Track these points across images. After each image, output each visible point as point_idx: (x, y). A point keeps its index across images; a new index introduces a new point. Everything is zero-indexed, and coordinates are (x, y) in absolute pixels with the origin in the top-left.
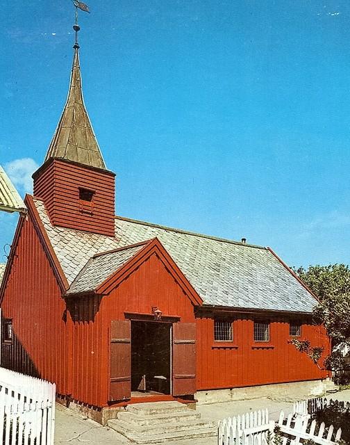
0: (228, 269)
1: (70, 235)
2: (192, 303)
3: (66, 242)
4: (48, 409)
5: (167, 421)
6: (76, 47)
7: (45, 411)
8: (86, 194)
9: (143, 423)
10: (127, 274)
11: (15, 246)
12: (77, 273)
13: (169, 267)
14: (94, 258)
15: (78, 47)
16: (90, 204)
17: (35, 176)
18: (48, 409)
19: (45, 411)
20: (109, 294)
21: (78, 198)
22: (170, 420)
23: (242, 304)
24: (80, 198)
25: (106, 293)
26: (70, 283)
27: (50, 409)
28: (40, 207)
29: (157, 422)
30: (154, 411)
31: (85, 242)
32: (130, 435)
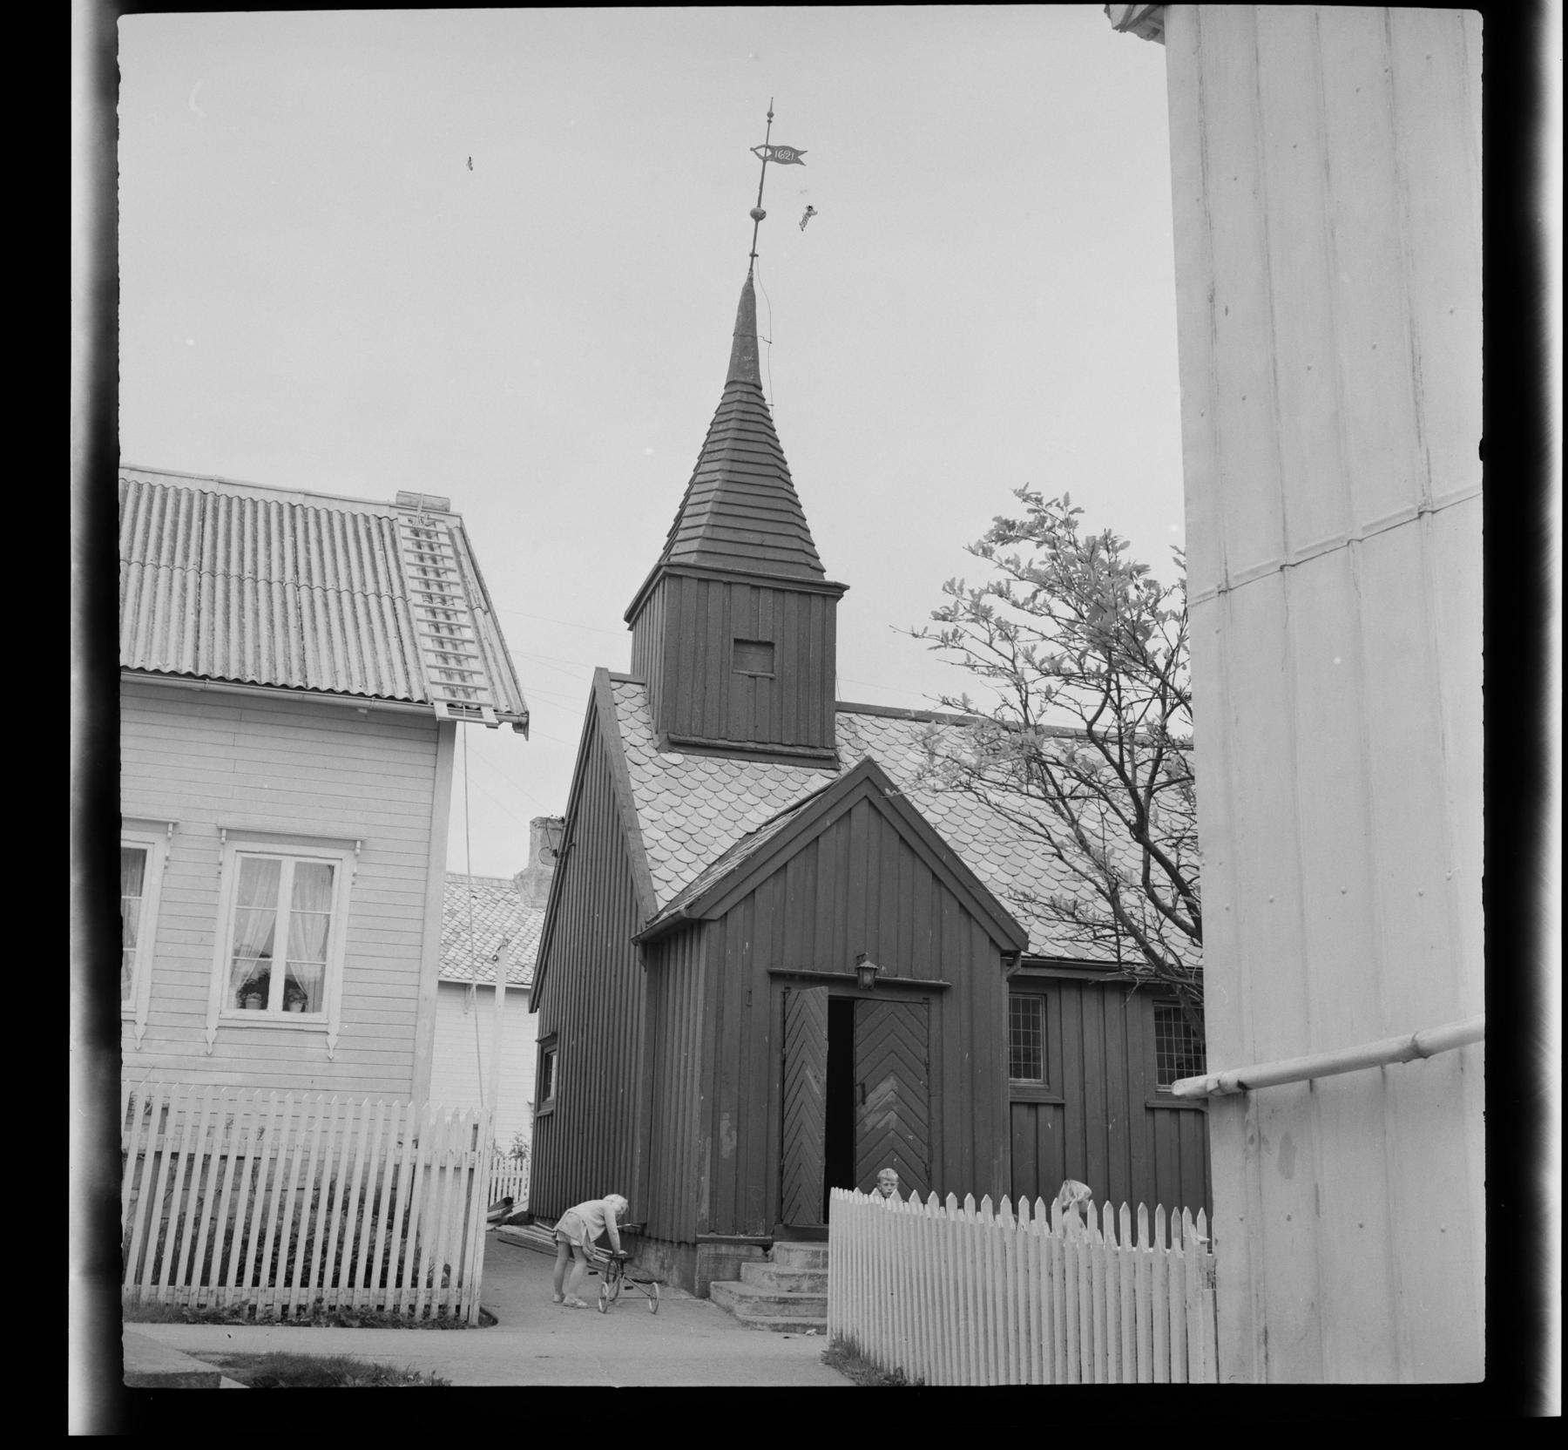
6: (758, 216)
25: (717, 913)
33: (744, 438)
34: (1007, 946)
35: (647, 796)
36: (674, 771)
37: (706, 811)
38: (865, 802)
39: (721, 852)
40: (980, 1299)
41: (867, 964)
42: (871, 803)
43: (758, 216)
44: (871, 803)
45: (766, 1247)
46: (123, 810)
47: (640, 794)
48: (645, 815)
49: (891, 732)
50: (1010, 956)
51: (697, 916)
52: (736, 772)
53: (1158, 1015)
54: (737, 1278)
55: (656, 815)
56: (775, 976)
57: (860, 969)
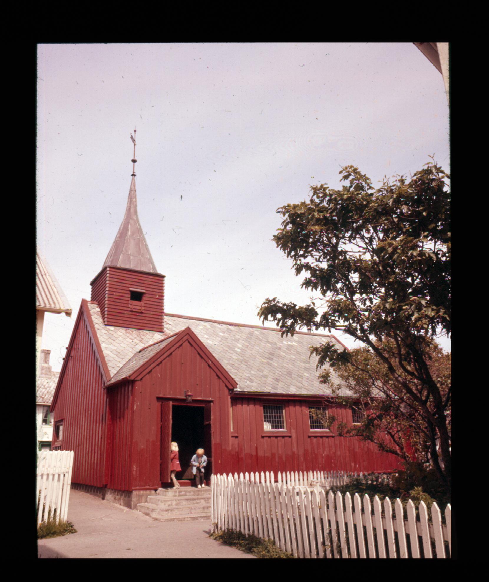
0: (283, 358)
1: (120, 332)
2: (226, 386)
3: (115, 339)
4: (64, 475)
5: (195, 502)
6: (133, 175)
7: (62, 476)
8: (137, 296)
9: (169, 503)
10: (159, 360)
11: (70, 349)
12: (121, 366)
13: (201, 353)
14: (140, 352)
15: (135, 175)
16: (142, 303)
17: (93, 283)
18: (64, 475)
19: (62, 476)
20: (141, 379)
21: (129, 299)
22: (198, 501)
23: (293, 390)
24: (131, 299)
25: (139, 378)
26: (112, 375)
27: (66, 475)
28: (94, 310)
29: (184, 502)
30: (183, 493)
31: (133, 338)
32: (154, 515)
33: (442, 73)
34: (231, 387)
35: (103, 340)
36: (111, 332)
37: (122, 345)
38: (187, 341)
39: (129, 358)
40: (97, 433)
41: (189, 394)
42: (189, 342)
43: (133, 175)
44: (189, 342)
45: (156, 490)
46: (37, 401)
47: (101, 339)
48: (103, 346)
49: (177, 321)
50: (231, 390)
51: (132, 379)
52: (131, 332)
53: (264, 408)
54: (146, 501)
55: (107, 346)
56: (158, 399)
57: (186, 396)
